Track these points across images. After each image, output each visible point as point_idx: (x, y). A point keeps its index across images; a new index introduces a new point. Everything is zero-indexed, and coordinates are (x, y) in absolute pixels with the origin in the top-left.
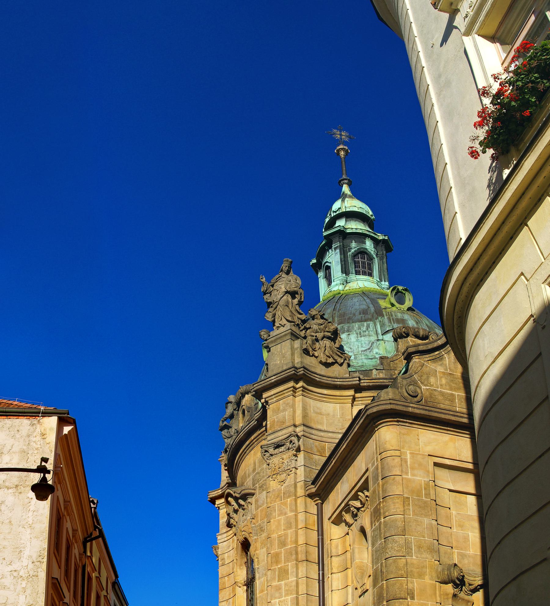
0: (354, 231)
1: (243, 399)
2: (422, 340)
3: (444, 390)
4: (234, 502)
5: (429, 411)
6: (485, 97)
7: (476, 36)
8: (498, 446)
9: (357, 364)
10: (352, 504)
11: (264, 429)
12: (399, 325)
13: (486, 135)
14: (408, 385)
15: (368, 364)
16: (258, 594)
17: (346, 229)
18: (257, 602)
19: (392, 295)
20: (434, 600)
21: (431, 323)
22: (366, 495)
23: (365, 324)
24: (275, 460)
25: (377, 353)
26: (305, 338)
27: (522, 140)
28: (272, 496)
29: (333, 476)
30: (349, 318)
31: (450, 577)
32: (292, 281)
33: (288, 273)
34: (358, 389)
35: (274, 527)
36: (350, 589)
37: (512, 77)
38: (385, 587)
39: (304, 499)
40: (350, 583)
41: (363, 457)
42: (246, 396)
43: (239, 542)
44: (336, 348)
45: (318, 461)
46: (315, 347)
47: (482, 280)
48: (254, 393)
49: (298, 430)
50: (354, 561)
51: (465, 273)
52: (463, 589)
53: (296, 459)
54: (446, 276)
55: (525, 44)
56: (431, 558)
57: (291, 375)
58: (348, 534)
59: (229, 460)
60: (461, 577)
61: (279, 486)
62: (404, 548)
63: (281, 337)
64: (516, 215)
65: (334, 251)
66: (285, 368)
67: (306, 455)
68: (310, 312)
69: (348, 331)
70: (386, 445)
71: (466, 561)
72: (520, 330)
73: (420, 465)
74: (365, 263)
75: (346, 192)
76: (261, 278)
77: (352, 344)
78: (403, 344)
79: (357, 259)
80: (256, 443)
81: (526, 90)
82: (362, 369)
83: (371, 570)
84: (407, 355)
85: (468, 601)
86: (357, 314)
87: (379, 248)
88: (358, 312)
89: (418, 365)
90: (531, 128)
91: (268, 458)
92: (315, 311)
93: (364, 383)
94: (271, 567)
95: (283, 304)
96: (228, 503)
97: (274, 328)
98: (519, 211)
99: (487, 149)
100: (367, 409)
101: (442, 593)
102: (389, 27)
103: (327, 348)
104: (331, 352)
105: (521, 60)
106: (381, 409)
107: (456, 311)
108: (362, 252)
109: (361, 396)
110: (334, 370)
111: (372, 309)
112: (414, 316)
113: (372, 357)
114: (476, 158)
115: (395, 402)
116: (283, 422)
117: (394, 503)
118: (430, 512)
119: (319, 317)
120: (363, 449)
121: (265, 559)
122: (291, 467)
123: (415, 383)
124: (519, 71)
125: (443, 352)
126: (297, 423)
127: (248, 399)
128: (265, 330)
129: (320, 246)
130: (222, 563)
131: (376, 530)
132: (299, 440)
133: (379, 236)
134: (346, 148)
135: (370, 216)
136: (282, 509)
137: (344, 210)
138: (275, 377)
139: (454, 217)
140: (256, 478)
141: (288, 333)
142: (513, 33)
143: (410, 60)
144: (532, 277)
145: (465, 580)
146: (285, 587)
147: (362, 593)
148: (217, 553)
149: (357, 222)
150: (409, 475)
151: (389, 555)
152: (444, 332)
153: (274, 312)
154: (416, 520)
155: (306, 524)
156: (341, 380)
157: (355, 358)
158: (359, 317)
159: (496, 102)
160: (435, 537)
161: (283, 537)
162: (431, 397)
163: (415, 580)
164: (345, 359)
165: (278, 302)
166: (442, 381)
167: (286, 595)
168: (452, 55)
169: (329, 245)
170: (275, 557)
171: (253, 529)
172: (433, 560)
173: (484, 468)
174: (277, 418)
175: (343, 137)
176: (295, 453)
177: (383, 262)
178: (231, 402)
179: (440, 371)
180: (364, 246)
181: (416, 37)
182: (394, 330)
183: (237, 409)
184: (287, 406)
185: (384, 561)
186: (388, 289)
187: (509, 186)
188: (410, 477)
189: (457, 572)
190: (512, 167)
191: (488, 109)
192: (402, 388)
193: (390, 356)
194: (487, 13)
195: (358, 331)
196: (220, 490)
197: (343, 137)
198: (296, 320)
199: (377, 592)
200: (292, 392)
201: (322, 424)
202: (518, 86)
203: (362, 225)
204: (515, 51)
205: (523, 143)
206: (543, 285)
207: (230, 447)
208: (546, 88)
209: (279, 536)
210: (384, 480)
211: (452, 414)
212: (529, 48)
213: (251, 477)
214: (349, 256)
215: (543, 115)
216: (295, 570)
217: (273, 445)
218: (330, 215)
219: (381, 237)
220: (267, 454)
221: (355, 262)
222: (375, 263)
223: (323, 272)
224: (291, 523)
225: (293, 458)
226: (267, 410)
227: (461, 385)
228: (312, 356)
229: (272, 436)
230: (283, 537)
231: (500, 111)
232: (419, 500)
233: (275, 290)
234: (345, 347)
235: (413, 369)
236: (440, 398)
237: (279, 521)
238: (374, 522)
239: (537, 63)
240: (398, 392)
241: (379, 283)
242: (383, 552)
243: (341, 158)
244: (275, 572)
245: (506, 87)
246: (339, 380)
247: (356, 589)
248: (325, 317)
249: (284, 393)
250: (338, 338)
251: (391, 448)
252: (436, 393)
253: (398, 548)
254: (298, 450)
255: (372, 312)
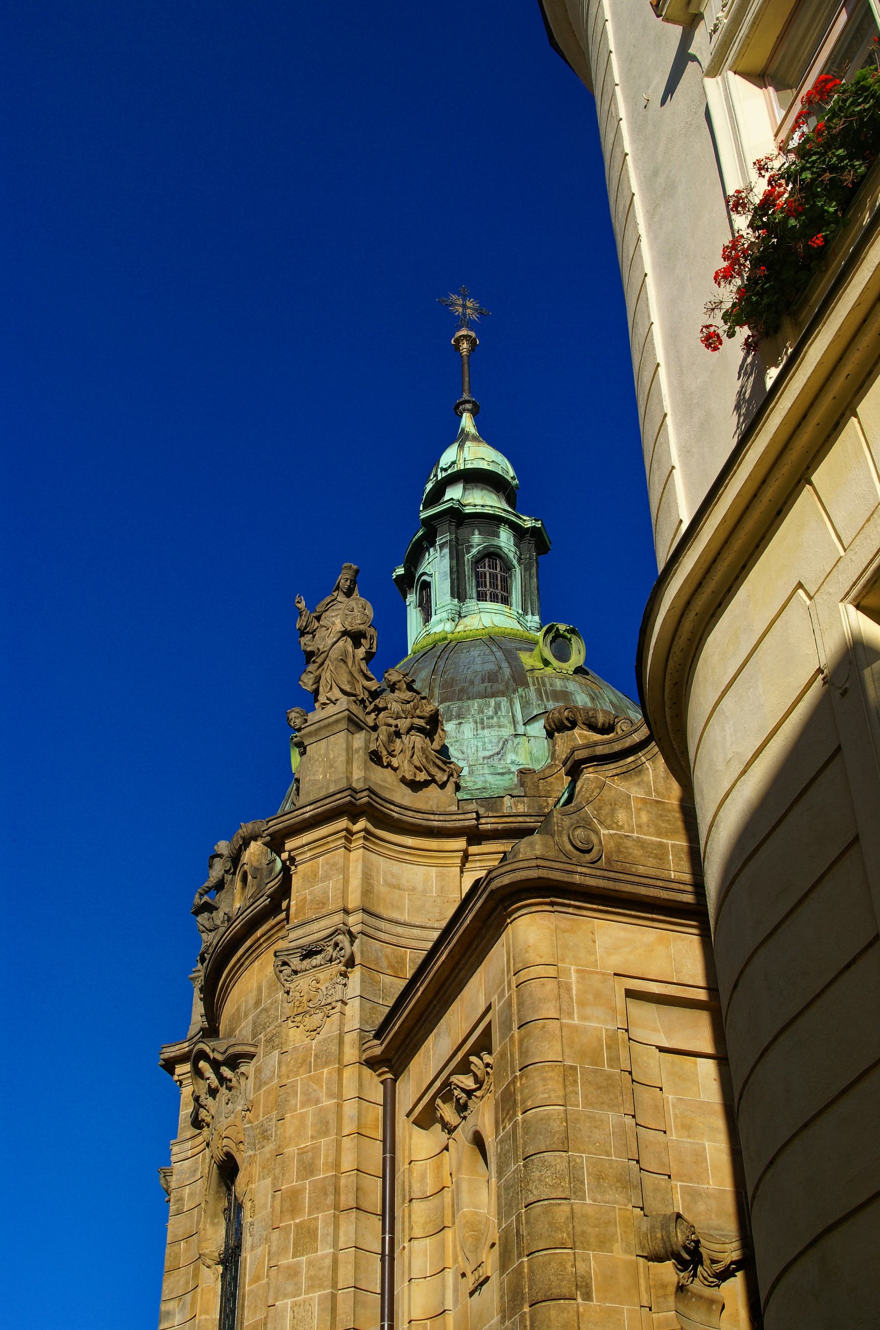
0: (479, 510)
1: (245, 850)
2: (603, 734)
3: (644, 837)
4: (211, 1071)
5: (615, 880)
6: (738, 213)
7: (730, 74)
8: (758, 948)
9: (474, 785)
10: (456, 1081)
11: (283, 915)
12: (557, 704)
13: (736, 298)
14: (574, 827)
15: (495, 785)
16: (248, 1286)
17: (463, 506)
18: (243, 1305)
19: (546, 642)
20: (636, 1300)
21: (619, 697)
22: (485, 1062)
23: (492, 702)
24: (303, 983)
25: (513, 763)
26: (375, 728)
27: (806, 300)
28: (292, 1061)
29: (418, 1021)
30: (462, 690)
31: (668, 1245)
32: (355, 610)
33: (349, 593)
34: (475, 836)
35: (292, 1129)
36: (449, 1275)
37: (794, 163)
38: (526, 1271)
39: (357, 1069)
40: (449, 1262)
41: (481, 979)
42: (253, 843)
43: (215, 1162)
44: (435, 751)
45: (390, 988)
46: (393, 749)
47: (719, 605)
48: (268, 838)
49: (352, 920)
50: (458, 1211)
51: (688, 591)
52: (698, 1273)
53: (344, 982)
54: (650, 600)
55: (822, 81)
56: (625, 1201)
57: (344, 805)
58: (447, 1148)
59: (207, 978)
60: (693, 1244)
61: (308, 1040)
62: (567, 1181)
63: (329, 725)
64: (789, 463)
65: (438, 551)
66: (332, 789)
67: (366, 973)
68: (386, 675)
69: (459, 716)
70: (527, 955)
71: (701, 1207)
72: (795, 704)
73: (598, 995)
74: (497, 576)
75: (467, 429)
76: (296, 601)
77: (466, 743)
78: (564, 743)
79: (481, 568)
80: (265, 945)
81: (819, 190)
82: (484, 794)
83: (496, 1231)
84: (572, 766)
85: (712, 1301)
86: (477, 681)
87: (524, 546)
88: (479, 677)
89: (593, 786)
90: (824, 272)
91: (287, 978)
92: (396, 674)
93: (487, 825)
94: (280, 1223)
95: (336, 656)
96: (198, 1073)
97: (317, 705)
98: (793, 455)
99: (737, 329)
100: (491, 879)
101: (652, 1283)
102: (571, 67)
103: (416, 750)
104: (424, 760)
105: (813, 121)
106: (519, 879)
107: (669, 671)
108: (492, 555)
109: (480, 852)
110: (428, 798)
111: (507, 671)
112: (586, 685)
113: (504, 770)
114: (716, 349)
115: (547, 864)
116: (324, 903)
117: (544, 1079)
118: (620, 1099)
119: (405, 686)
120: (481, 964)
121: (267, 1203)
122: (334, 999)
123: (587, 824)
124: (807, 147)
125: (642, 758)
126: (350, 906)
127: (255, 851)
128: (297, 709)
129: (414, 540)
130: (178, 1209)
131: (506, 1140)
132: (352, 943)
133: (525, 521)
134: (473, 334)
135: (510, 480)
136: (311, 1090)
137: (462, 468)
138: (312, 807)
139: (669, 476)
140: (260, 1020)
141: (343, 718)
142: (802, 60)
143: (602, 140)
144: (820, 591)
145: (702, 1250)
146: (308, 1269)
147: (476, 1285)
148: (167, 1185)
149: (485, 492)
150: (576, 1019)
151: (534, 1195)
152: (645, 715)
153: (318, 672)
154: (590, 1117)
155: (359, 1126)
156: (441, 818)
157: (471, 773)
158: (480, 687)
159: (760, 223)
160: (632, 1155)
161: (310, 1154)
162: (619, 851)
163: (591, 1252)
164: (451, 775)
165: (326, 653)
166: (640, 818)
167: (310, 1289)
168: (682, 124)
169: (429, 540)
170: (291, 1199)
171: (247, 1134)
172: (630, 1207)
173: (731, 998)
174: (310, 894)
175: (469, 311)
176: (344, 968)
177: (530, 574)
178: (220, 856)
179: (637, 798)
180: (495, 542)
181: (617, 85)
182: (547, 714)
183: (232, 871)
184: (332, 870)
185: (524, 1211)
186: (539, 629)
187: (777, 403)
188: (576, 1022)
189: (683, 1232)
190: (784, 362)
191: (743, 240)
192: (560, 834)
193: (539, 767)
194: (755, 17)
195: (478, 718)
196: (187, 1044)
197: (469, 311)
198: (359, 691)
199: (510, 1282)
200: (343, 841)
201: (400, 908)
202: (804, 181)
203: (495, 497)
204: (802, 102)
205: (808, 308)
206: (841, 606)
207: (211, 950)
208: (859, 178)
209: (300, 1151)
210: (523, 1030)
211: (661, 885)
212: (830, 89)
213: (250, 1017)
214: (466, 563)
215: (849, 240)
216: (331, 1230)
217: (300, 950)
218: (436, 475)
219: (528, 523)
220: (287, 970)
221: (477, 573)
222: (515, 576)
223: (416, 594)
224: (328, 1122)
225: (339, 980)
226: (291, 875)
227: (680, 824)
228: (387, 767)
229: (299, 932)
230: (310, 1154)
231: (766, 242)
232: (595, 1072)
233: (322, 626)
234: (452, 751)
235: (583, 793)
236: (637, 852)
237: (303, 1117)
238: (503, 1121)
239: (845, 122)
240: (552, 843)
241: (521, 618)
242: (521, 1191)
243: (462, 357)
244: (288, 1234)
245: (780, 185)
246: (436, 817)
247: (463, 1275)
248: (415, 687)
249: (328, 842)
250: (439, 731)
251: (539, 961)
252: (629, 843)
253: (554, 1181)
254: (350, 963)
255: (506, 677)
